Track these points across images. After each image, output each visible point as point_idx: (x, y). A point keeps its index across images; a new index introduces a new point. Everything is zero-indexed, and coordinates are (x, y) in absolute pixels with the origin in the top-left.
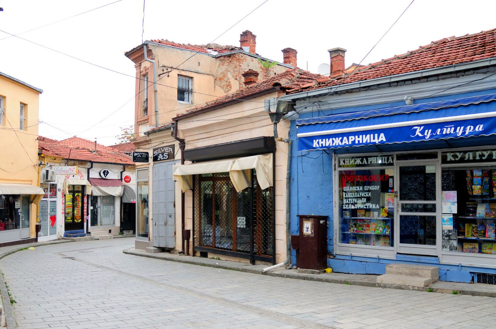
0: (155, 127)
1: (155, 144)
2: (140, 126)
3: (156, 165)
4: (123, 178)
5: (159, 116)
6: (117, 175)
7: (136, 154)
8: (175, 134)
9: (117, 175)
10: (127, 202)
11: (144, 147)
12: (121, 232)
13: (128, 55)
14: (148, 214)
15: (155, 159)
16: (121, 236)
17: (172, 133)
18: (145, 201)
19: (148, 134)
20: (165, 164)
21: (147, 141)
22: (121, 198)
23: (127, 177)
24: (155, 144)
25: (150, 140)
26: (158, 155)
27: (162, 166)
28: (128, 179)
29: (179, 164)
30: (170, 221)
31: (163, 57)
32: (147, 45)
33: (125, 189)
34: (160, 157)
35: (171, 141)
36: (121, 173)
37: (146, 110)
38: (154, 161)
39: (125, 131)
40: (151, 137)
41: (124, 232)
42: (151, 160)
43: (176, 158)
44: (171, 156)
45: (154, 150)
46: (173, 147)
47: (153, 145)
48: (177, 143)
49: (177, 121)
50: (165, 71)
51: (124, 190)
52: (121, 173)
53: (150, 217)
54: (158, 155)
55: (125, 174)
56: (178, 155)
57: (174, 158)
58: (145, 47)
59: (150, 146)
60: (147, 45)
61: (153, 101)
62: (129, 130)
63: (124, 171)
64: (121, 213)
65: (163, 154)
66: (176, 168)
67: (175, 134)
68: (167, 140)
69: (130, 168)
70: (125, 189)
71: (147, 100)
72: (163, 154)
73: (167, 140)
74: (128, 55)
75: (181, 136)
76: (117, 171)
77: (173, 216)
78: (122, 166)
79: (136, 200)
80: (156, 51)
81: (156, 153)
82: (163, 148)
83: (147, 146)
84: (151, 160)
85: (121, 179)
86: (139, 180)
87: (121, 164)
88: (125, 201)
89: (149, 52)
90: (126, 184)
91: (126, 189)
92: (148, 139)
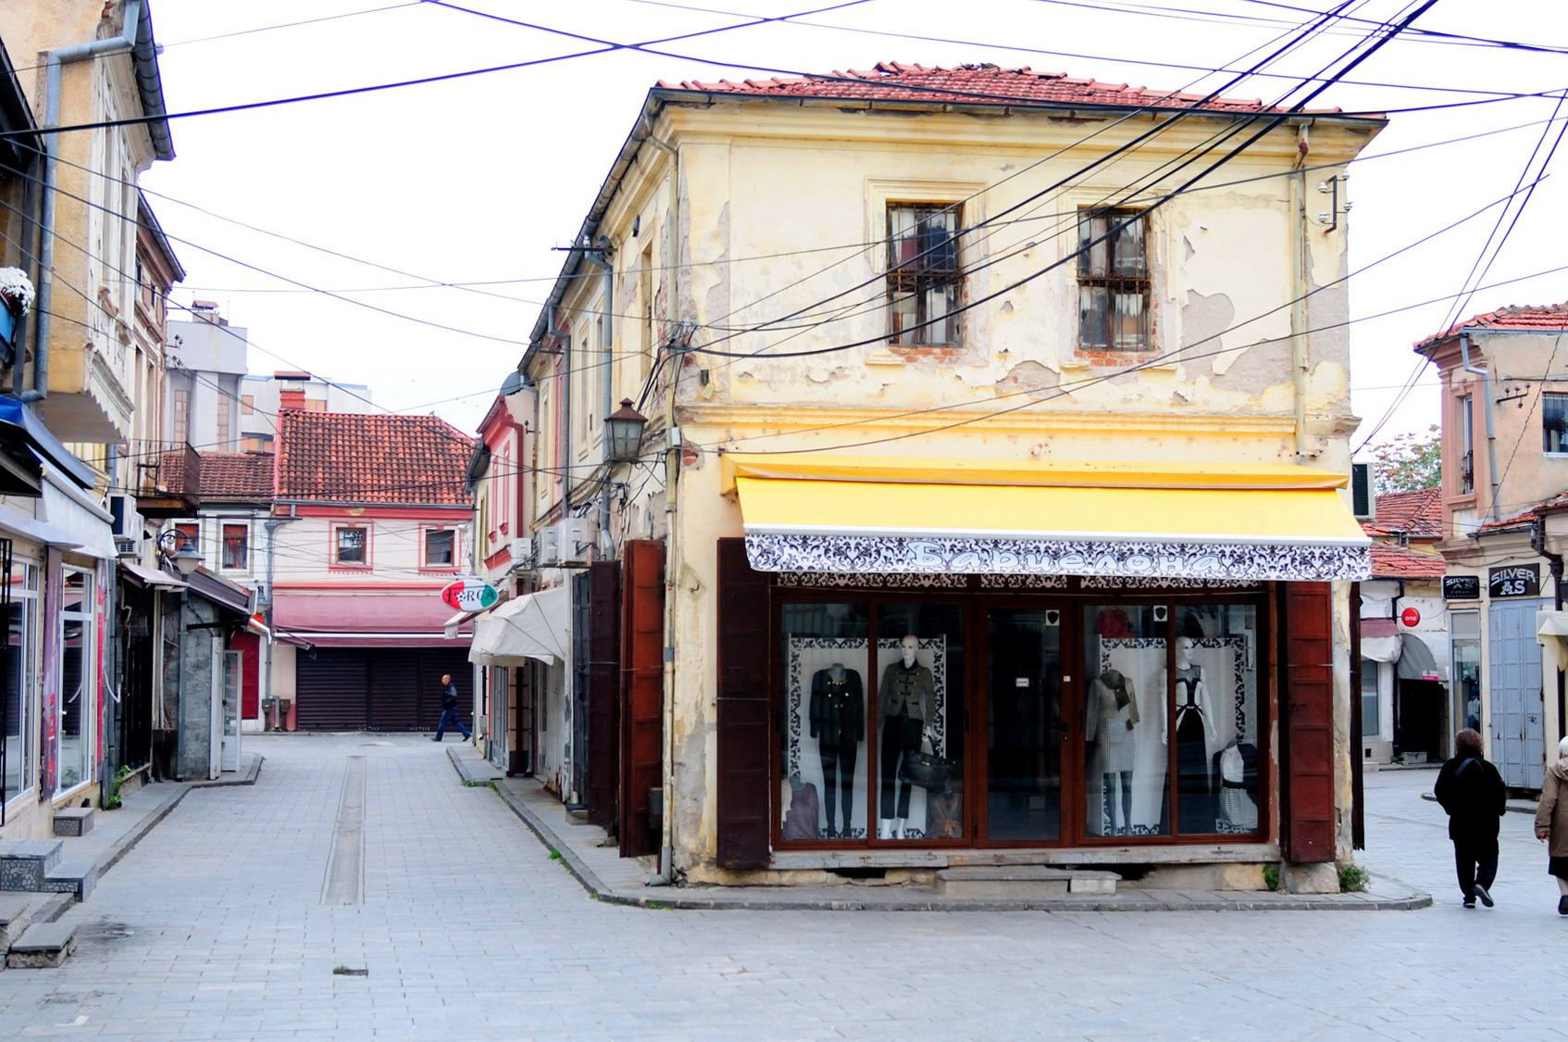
0: (1490, 521)
1: (1493, 558)
2: (1456, 515)
3: (1497, 607)
4: (1399, 613)
5: (1502, 492)
6: (1383, 606)
7: (1449, 582)
8: (1540, 544)
9: (1383, 606)
10: (1409, 676)
11: (1467, 562)
12: (1397, 755)
13: (1419, 349)
14: (1479, 711)
15: (1495, 591)
16: (1395, 765)
17: (1534, 541)
18: (1471, 687)
19: (1477, 536)
20: (1519, 604)
21: (1475, 550)
22: (1395, 666)
23: (1409, 612)
24: (1493, 558)
25: (1482, 549)
26: (1501, 584)
27: (1513, 609)
28: (1412, 618)
29: (1550, 608)
30: (1533, 731)
31: (1507, 356)
32: (1467, 336)
33: (1406, 642)
34: (1507, 587)
35: (1532, 557)
36: (1394, 601)
37: (1469, 477)
38: (1492, 595)
39: (1379, 453)
40: (1483, 543)
41: (1405, 755)
42: (1484, 594)
43: (1543, 594)
44: (1532, 589)
45: (1492, 571)
46: (1536, 568)
47: (1489, 560)
48: (1545, 565)
49: (1543, 517)
50: (1513, 393)
51: (1403, 645)
52: (1394, 601)
53: (1486, 720)
54: (1501, 584)
55: (1404, 604)
56: (1548, 588)
57: (1538, 592)
58: (1463, 341)
59: (1481, 561)
60: (1467, 336)
61: (1487, 460)
62: (1392, 450)
63: (1402, 595)
64: (1395, 706)
65: (1512, 582)
66: (1544, 619)
67: (1540, 544)
68: (1521, 554)
69: (1415, 588)
70: (1406, 642)
71: (1471, 454)
72: (1512, 582)
73: (1521, 554)
74: (1419, 349)
75: (1553, 548)
76: (1383, 596)
77: (1539, 720)
78: (1396, 584)
79: (1444, 672)
80: (1489, 347)
81: (1497, 579)
82: (1512, 568)
83: (1474, 561)
84: (1484, 594)
85: (1394, 617)
86: (1456, 637)
87: (1392, 579)
88: (1406, 674)
89: (1474, 350)
90: (1407, 629)
91: (1409, 643)
92: (1476, 546)
